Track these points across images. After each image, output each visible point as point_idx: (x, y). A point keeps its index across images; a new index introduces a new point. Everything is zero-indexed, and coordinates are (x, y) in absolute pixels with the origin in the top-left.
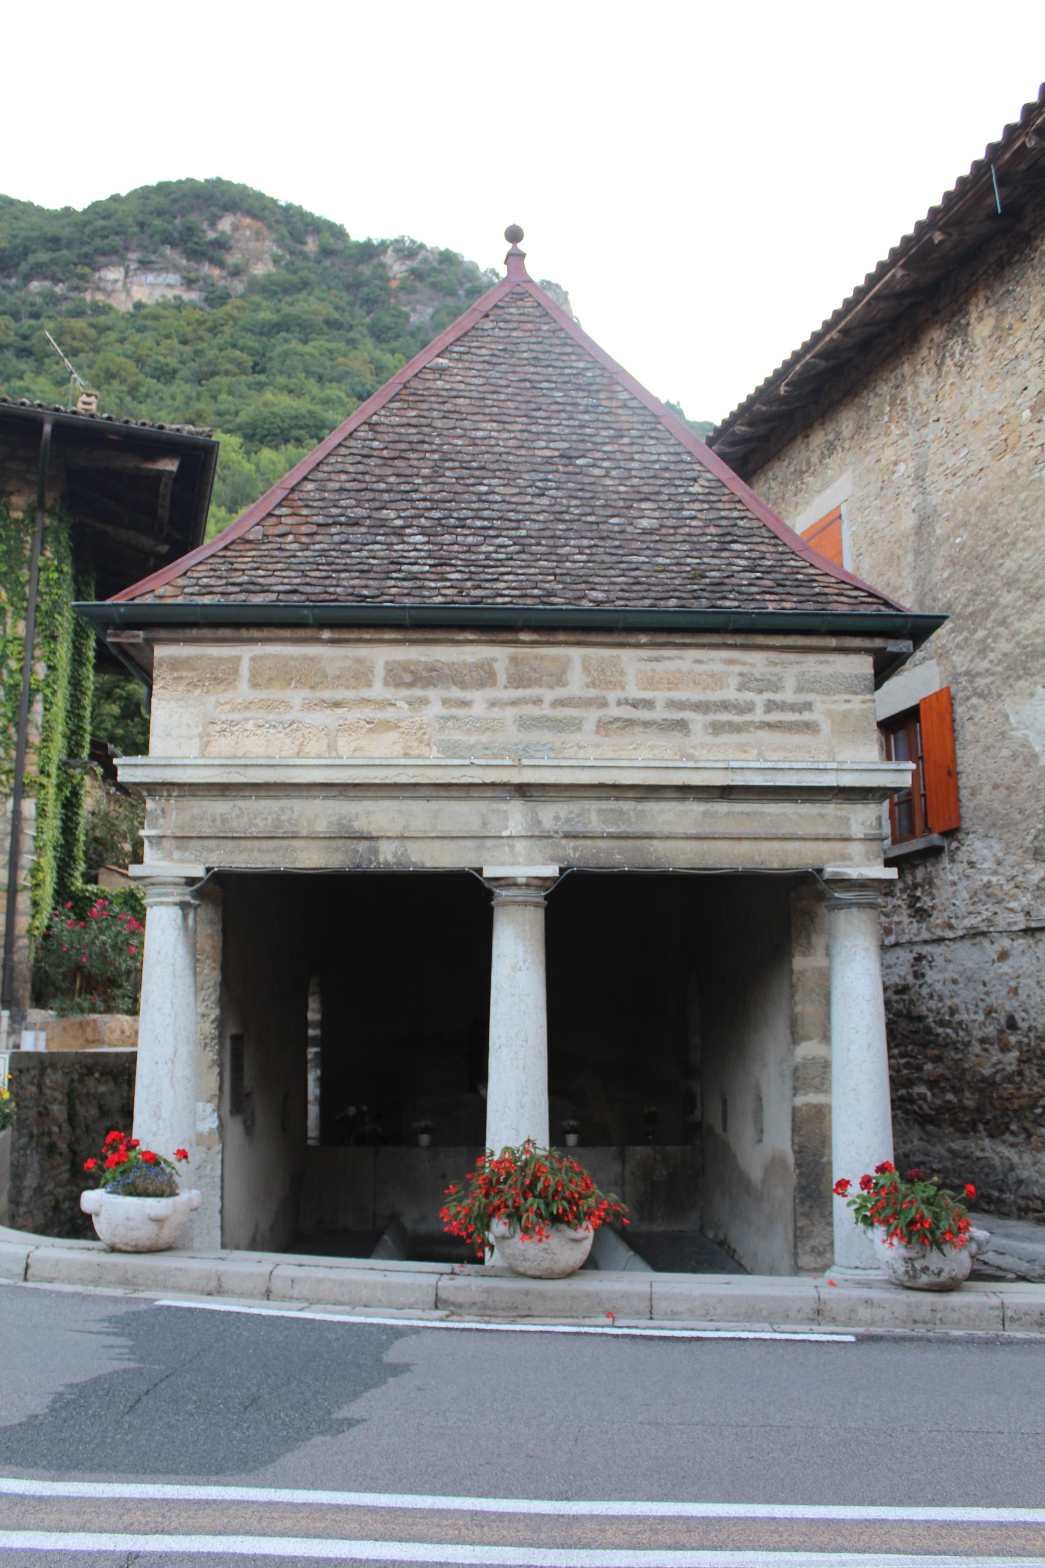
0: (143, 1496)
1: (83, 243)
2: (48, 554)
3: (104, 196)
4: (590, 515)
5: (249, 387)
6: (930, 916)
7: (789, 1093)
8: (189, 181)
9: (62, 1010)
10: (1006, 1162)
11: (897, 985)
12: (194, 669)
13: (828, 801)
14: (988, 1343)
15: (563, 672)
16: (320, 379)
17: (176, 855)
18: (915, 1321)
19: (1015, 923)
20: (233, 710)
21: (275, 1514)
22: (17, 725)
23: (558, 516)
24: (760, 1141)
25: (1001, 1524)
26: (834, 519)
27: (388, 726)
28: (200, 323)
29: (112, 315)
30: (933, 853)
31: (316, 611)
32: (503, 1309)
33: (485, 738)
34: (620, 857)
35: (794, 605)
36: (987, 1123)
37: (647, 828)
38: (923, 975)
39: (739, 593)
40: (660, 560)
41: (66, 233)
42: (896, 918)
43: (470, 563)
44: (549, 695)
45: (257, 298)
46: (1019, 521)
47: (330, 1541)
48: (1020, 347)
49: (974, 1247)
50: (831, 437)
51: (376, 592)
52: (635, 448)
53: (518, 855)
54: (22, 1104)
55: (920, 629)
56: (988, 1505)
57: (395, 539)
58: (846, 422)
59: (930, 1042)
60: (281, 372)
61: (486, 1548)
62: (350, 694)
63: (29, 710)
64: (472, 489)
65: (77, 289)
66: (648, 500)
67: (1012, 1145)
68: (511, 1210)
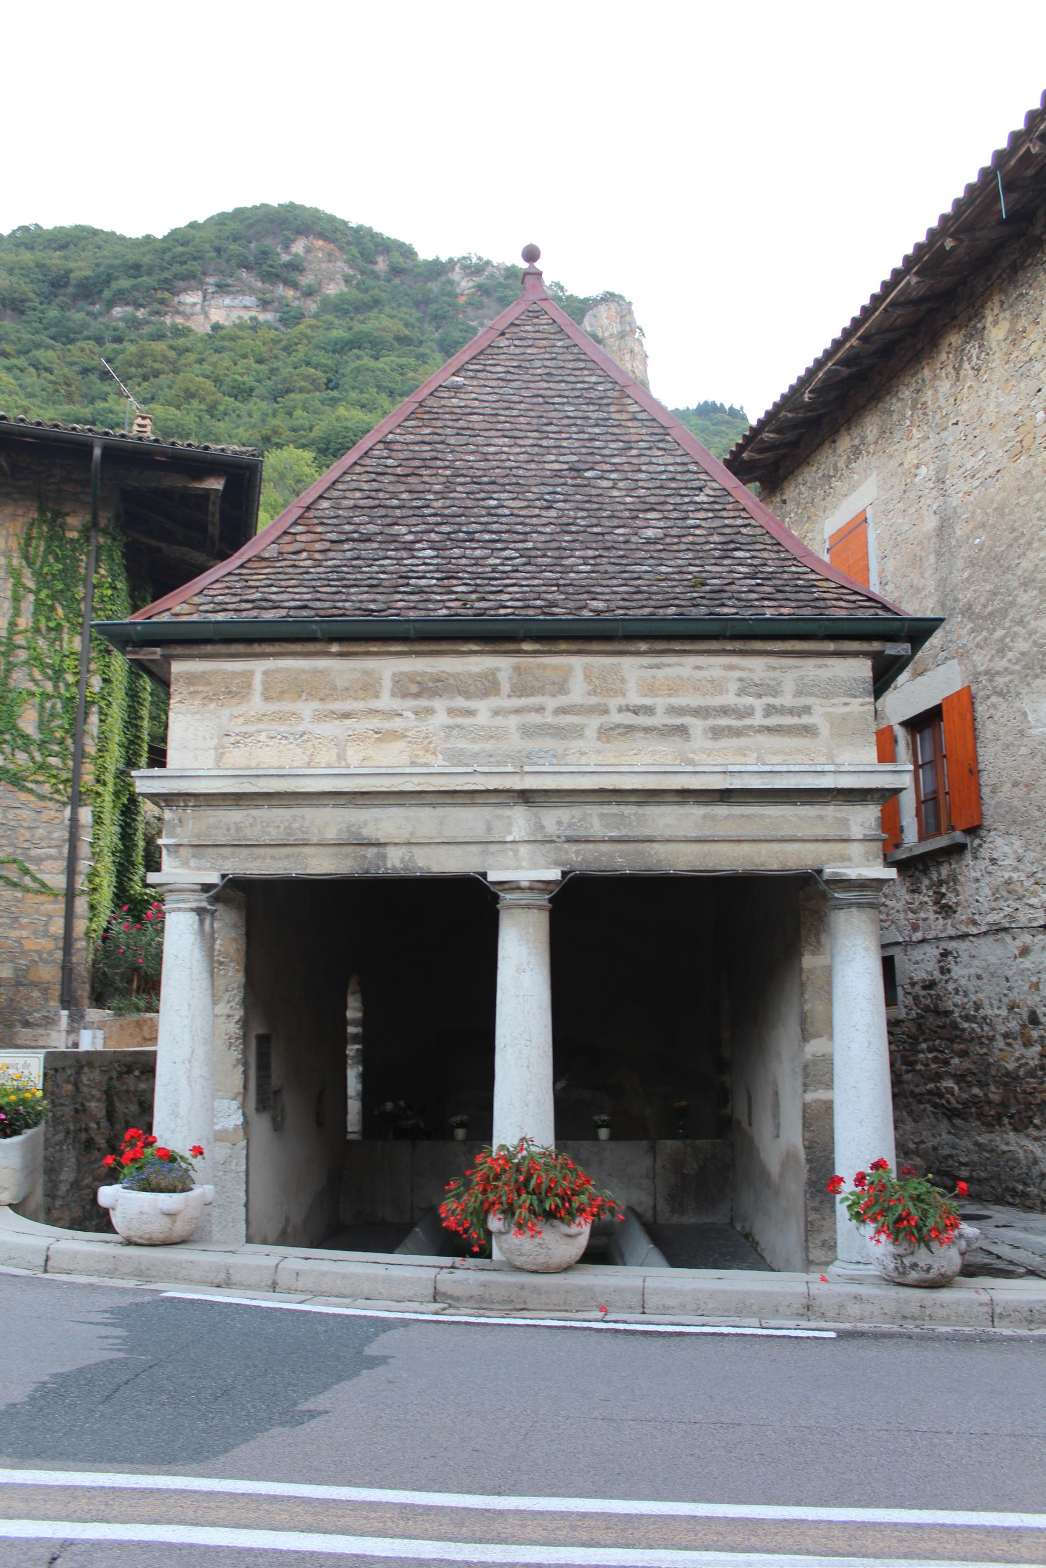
0: (93, 1484)
1: (163, 269)
2: (103, 572)
3: (182, 223)
4: (596, 526)
5: (323, 403)
6: (955, 912)
7: (800, 1089)
8: (264, 206)
9: (120, 1009)
10: (1030, 1156)
11: (924, 980)
12: (209, 684)
13: (827, 803)
14: (967, 1340)
15: (565, 681)
16: (391, 394)
17: (193, 863)
18: (905, 1317)
19: (1035, 919)
20: (245, 723)
21: (212, 1505)
22: (73, 736)
23: (565, 528)
24: (778, 1136)
25: (918, 1526)
26: (860, 522)
27: (395, 735)
28: (275, 342)
29: (191, 338)
30: (956, 850)
31: (324, 625)
32: (498, 1303)
33: (489, 746)
34: (621, 860)
35: (792, 611)
36: (1011, 1117)
37: (647, 832)
38: (949, 971)
39: (738, 599)
40: (663, 569)
41: (146, 260)
42: (922, 915)
43: (477, 576)
44: (552, 703)
45: (329, 317)
46: (1035, 522)
47: (258, 1532)
48: (1033, 349)
49: (963, 1244)
50: (856, 442)
51: (384, 606)
52: (643, 459)
53: (521, 860)
54: (57, 1101)
55: (919, 632)
56: (911, 1507)
57: (404, 554)
58: (871, 427)
59: (957, 1037)
60: (353, 388)
61: (406, 1541)
62: (359, 706)
63: (85, 721)
64: (482, 503)
65: (157, 313)
66: (654, 510)
67: (1036, 1139)
68: (505, 1207)
